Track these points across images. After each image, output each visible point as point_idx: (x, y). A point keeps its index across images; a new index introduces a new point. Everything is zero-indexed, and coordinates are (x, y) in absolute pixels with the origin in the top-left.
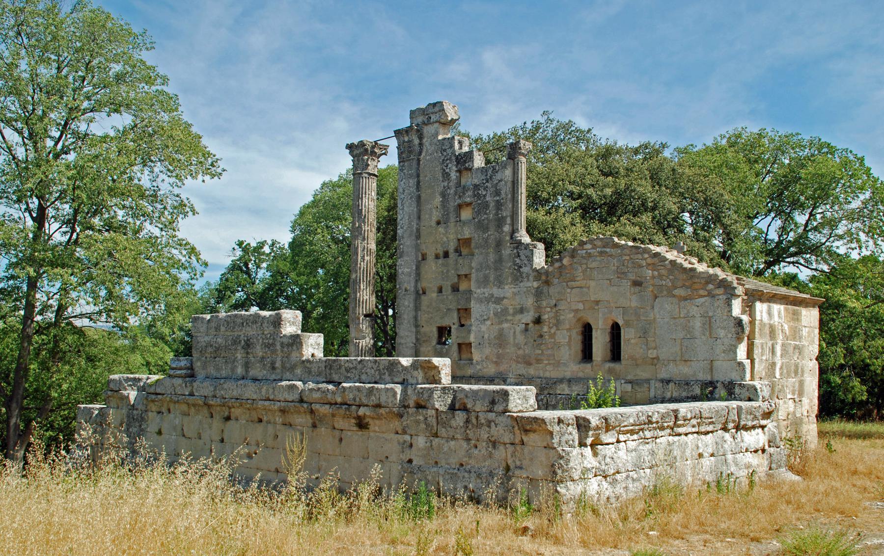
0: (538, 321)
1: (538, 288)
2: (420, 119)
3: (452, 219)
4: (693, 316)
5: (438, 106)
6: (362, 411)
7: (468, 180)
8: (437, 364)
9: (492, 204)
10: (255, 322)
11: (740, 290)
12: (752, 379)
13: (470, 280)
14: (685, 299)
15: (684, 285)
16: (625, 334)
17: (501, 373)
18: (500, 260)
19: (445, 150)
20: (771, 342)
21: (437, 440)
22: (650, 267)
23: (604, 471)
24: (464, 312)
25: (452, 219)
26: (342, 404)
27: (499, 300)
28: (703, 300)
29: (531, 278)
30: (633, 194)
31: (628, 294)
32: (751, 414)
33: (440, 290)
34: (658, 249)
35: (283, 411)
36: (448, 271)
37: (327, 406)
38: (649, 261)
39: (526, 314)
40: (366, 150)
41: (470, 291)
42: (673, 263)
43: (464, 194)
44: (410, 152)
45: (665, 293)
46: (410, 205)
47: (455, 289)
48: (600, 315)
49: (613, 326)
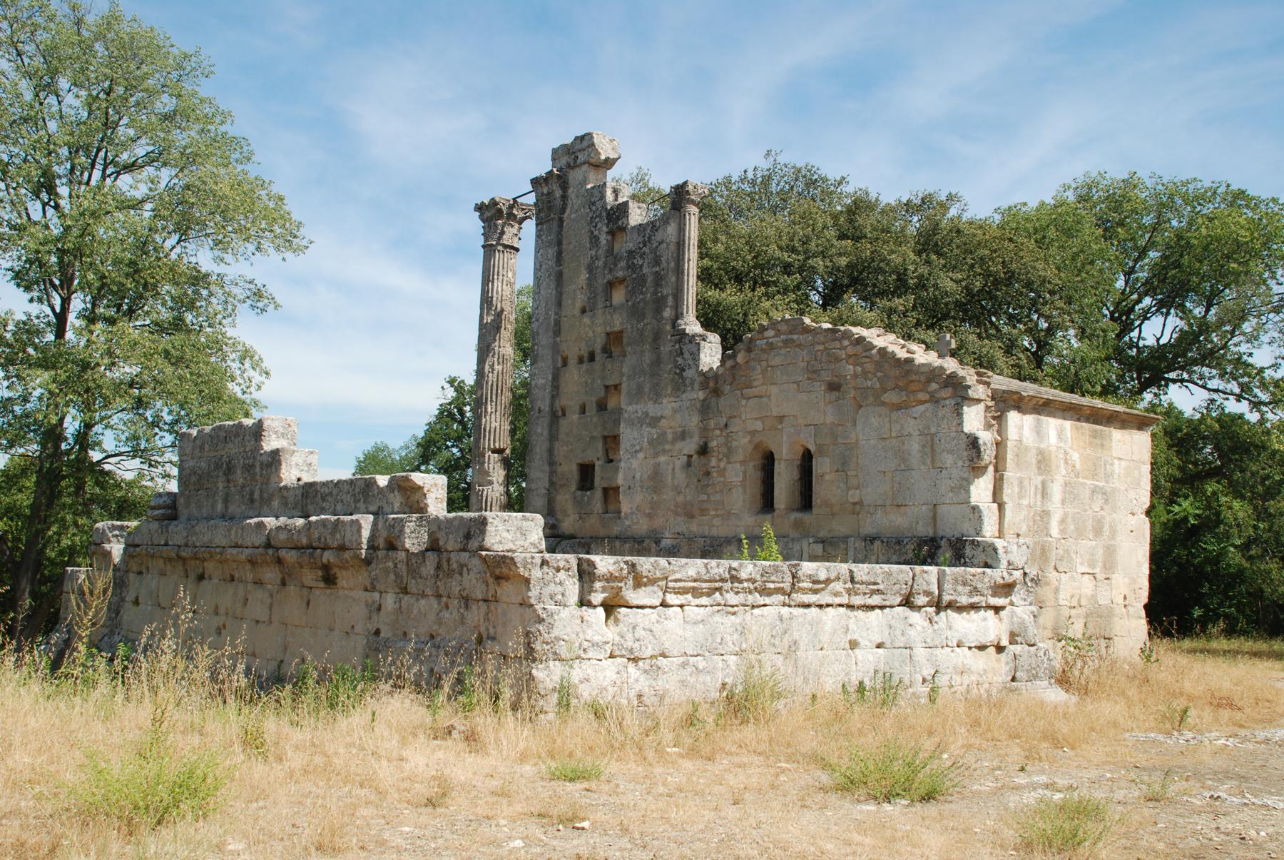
0: (704, 450)
1: (705, 400)
2: (564, 161)
3: (600, 304)
4: (910, 435)
5: (585, 141)
6: (328, 556)
7: (625, 244)
8: (420, 483)
9: (650, 279)
10: (237, 435)
11: (979, 391)
12: (1001, 535)
13: (620, 392)
14: (898, 407)
15: (897, 386)
16: (821, 467)
17: (654, 531)
18: (657, 362)
19: (594, 204)
20: (1040, 478)
21: (406, 598)
22: (851, 361)
23: (631, 651)
24: (612, 441)
25: (600, 304)
26: (308, 547)
27: (655, 421)
28: (922, 408)
29: (696, 386)
30: (882, 265)
31: (822, 403)
32: (964, 584)
33: (583, 410)
34: (864, 332)
35: (252, 562)
36: (593, 380)
37: (293, 552)
38: (850, 350)
39: (688, 440)
40: (500, 211)
41: (619, 411)
42: (883, 351)
43: (616, 265)
44: (550, 209)
45: (871, 399)
46: (548, 285)
47: (602, 406)
48: (785, 438)
49: (804, 455)
